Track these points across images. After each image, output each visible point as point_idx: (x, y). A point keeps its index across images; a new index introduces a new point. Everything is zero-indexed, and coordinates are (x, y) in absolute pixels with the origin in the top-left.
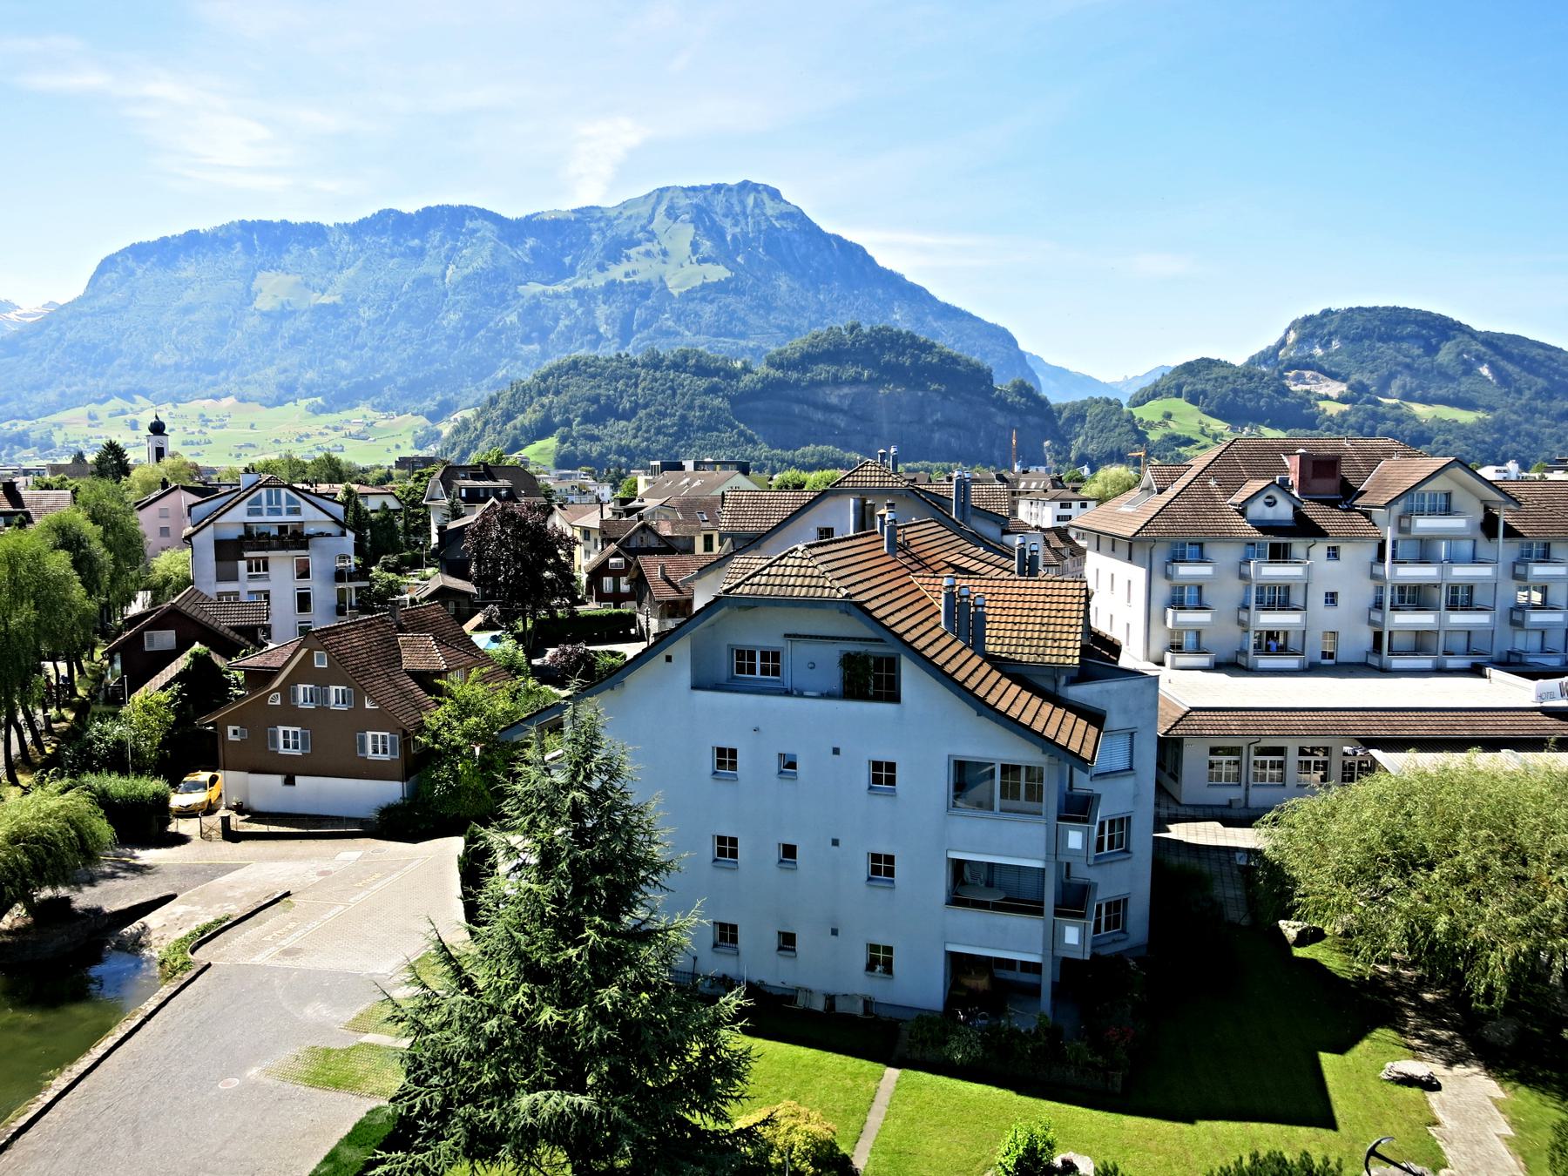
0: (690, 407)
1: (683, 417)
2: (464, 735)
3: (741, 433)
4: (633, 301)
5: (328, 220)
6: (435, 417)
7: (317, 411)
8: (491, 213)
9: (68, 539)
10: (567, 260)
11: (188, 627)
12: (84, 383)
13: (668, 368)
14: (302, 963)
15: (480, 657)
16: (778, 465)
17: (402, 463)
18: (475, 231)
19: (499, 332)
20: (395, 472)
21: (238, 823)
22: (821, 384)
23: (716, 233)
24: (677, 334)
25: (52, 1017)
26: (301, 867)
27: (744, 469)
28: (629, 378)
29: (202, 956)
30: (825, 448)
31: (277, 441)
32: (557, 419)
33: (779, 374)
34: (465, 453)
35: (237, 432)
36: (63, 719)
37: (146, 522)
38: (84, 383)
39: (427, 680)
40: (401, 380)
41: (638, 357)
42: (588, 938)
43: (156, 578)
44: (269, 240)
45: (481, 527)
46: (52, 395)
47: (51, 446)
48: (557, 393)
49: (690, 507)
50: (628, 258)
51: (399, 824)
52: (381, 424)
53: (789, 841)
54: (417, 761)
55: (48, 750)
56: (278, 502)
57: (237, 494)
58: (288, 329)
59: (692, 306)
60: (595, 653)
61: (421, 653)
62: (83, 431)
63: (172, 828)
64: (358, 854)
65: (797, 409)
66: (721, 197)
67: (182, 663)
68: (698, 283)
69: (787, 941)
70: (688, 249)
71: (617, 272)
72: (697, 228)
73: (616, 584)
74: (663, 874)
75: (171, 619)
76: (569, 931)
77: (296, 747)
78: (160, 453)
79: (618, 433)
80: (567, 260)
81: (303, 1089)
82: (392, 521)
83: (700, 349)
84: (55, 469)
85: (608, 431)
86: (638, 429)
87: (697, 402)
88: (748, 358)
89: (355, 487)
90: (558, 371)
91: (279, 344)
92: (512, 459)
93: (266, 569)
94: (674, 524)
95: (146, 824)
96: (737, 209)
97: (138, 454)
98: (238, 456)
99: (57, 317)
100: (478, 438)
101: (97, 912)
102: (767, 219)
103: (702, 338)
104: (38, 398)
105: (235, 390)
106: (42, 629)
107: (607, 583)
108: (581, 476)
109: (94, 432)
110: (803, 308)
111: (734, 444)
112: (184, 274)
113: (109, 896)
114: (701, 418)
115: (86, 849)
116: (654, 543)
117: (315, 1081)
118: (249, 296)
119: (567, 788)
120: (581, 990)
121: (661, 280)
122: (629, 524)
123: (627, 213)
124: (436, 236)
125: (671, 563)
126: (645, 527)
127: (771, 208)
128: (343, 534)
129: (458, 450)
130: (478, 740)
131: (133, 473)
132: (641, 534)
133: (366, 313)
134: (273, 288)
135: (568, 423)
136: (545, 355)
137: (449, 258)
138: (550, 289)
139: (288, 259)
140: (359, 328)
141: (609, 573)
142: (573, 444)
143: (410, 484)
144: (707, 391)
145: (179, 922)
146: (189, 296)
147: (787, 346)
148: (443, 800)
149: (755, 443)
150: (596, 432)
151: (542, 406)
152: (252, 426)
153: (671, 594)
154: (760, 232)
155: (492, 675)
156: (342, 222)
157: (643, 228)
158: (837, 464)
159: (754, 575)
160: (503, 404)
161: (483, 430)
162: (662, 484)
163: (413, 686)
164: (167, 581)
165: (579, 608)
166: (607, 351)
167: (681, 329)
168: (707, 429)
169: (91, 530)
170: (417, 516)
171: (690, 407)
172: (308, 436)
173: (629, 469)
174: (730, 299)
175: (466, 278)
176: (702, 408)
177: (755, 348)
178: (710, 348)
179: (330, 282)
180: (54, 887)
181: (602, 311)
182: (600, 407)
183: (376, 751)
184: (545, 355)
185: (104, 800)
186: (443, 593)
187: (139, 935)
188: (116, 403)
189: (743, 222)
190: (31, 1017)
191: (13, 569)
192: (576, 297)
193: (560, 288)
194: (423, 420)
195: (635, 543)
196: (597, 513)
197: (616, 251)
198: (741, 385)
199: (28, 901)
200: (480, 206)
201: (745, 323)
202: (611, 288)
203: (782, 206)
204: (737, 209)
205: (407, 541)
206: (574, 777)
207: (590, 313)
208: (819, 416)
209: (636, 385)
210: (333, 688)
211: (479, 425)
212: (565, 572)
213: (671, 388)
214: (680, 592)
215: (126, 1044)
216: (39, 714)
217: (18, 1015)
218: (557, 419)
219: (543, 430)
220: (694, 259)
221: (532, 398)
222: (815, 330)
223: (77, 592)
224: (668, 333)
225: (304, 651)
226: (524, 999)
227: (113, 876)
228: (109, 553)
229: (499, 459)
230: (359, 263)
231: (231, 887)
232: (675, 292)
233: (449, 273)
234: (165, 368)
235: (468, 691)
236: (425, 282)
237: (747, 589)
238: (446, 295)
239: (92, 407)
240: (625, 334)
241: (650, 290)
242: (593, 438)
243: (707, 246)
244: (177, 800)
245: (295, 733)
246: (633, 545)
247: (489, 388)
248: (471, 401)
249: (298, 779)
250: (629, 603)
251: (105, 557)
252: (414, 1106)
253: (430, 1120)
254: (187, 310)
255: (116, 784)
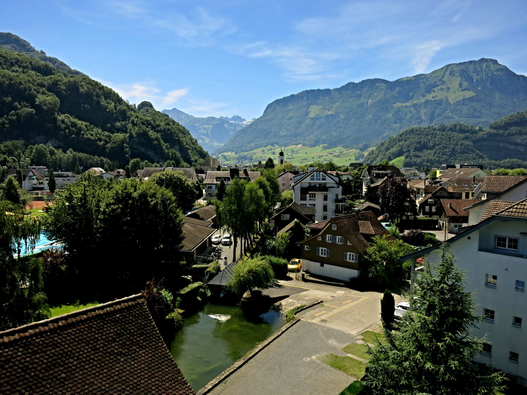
0: (457, 145)
1: (453, 149)
2: (381, 257)
3: (477, 154)
4: (435, 107)
5: (332, 88)
6: (362, 150)
7: (325, 148)
8: (384, 80)
9: (261, 185)
10: (411, 94)
11: (293, 213)
12: (261, 141)
13: (448, 130)
14: (328, 325)
15: (387, 232)
16: (493, 167)
17: (352, 165)
18: (379, 87)
19: (386, 120)
20: (349, 168)
21: (307, 276)
22: (513, 135)
23: (470, 79)
24: (452, 117)
25: (256, 326)
26: (326, 293)
27: (481, 167)
28: (433, 135)
29: (297, 316)
30: (514, 160)
31: (313, 158)
32: (405, 150)
33: (495, 131)
34: (372, 162)
35: (302, 155)
36: (257, 238)
37: (280, 181)
38: (261, 141)
39: (368, 237)
40: (352, 138)
41: (435, 127)
42: (446, 340)
43: (282, 198)
44: (312, 96)
45: (384, 186)
46: (253, 145)
47: (252, 159)
48: (405, 141)
49: (460, 181)
50: (434, 91)
51: (358, 285)
52: (345, 152)
53: (519, 316)
54: (363, 264)
55: (254, 247)
56: (319, 176)
57: (306, 174)
58: (318, 123)
59: (458, 107)
60: (424, 233)
61: (366, 228)
62: (262, 155)
63: (288, 275)
64: (343, 292)
65: (502, 145)
66: (472, 65)
67: (292, 224)
68: (462, 98)
69: (514, 356)
70: (458, 86)
71: (429, 97)
72: (462, 78)
73: (431, 209)
74: (475, 321)
75: (290, 211)
76: (438, 336)
77: (325, 254)
78: (282, 162)
79: (427, 155)
80: (411, 94)
81: (329, 367)
82: (350, 183)
83: (461, 123)
84: (255, 166)
85: (424, 154)
86: (436, 153)
87: (459, 143)
88: (481, 125)
89: (339, 172)
90: (406, 133)
91: (315, 128)
92: (391, 163)
93: (315, 197)
94: (454, 188)
95: (282, 273)
96: (479, 69)
97: (276, 162)
98: (302, 162)
99: (256, 122)
100: (377, 156)
101: (268, 297)
102: (491, 72)
103: (462, 119)
104: (250, 146)
105: (302, 142)
106: (256, 212)
107: (427, 208)
108: (414, 170)
109: (263, 155)
110: (506, 105)
111: (474, 159)
112: (289, 108)
113: (271, 292)
114: (460, 149)
115: (267, 278)
116: (446, 194)
117: (332, 365)
118: (307, 113)
119: (440, 282)
120: (441, 359)
121: (446, 98)
122: (436, 188)
123: (434, 75)
124: (365, 89)
125: (454, 202)
126: (442, 189)
127: (493, 67)
128: (338, 187)
129: (370, 161)
130: (385, 260)
131: (276, 167)
132: (440, 191)
133: (342, 116)
134: (314, 110)
135: (409, 151)
136: (401, 128)
137: (369, 97)
138: (404, 105)
139: (319, 101)
140: (339, 121)
141: (428, 205)
142: (410, 158)
143: (356, 171)
144: (463, 139)
145: (291, 304)
146: (291, 114)
147: (498, 120)
148: (372, 279)
149: (483, 158)
150: (419, 154)
151: (400, 145)
152: (306, 153)
153: (453, 214)
154: (488, 77)
155: (389, 237)
156: (336, 88)
157: (440, 80)
158: (519, 166)
159: (510, 208)
160: (386, 145)
161: (379, 154)
162: (448, 173)
163: (363, 239)
164: (285, 199)
165: (418, 217)
166: (424, 125)
167: (454, 116)
168: (463, 153)
169: (267, 183)
170: (358, 182)
171: (457, 145)
172: (322, 156)
173: (431, 167)
174: (474, 104)
175: (375, 103)
176: (461, 145)
177: (484, 121)
178: (465, 123)
179: (331, 107)
180: (258, 287)
181: (423, 111)
182: (421, 145)
183: (350, 259)
184: (401, 128)
185: (271, 263)
186: (368, 208)
187: (279, 306)
188: (270, 147)
189: (481, 74)
190: (251, 325)
191: (251, 194)
192: (413, 107)
193: (408, 104)
194: (358, 151)
195: (438, 195)
196: (423, 183)
197: (429, 90)
198: (478, 136)
199: (251, 290)
200: (381, 78)
201: (480, 112)
202: (427, 102)
203: (498, 67)
204: (479, 69)
205: (355, 190)
206: (443, 278)
207: (418, 112)
208: (512, 147)
209: (435, 137)
210: (338, 237)
211: (377, 152)
212: (413, 202)
213: (449, 138)
214: (457, 213)
215: (277, 339)
216: (252, 237)
217: (248, 323)
218: (405, 150)
219: (399, 154)
220: (460, 90)
221: (396, 143)
222: (511, 114)
223: (264, 202)
224: (448, 118)
225: (329, 224)
226: (420, 357)
227: (272, 287)
228: (272, 190)
229: (387, 163)
230: (340, 101)
231: (305, 296)
232: (452, 103)
233: (369, 101)
234: (283, 136)
235: (382, 242)
236: (362, 105)
237: (506, 213)
238: (368, 109)
239: (263, 148)
240: (432, 119)
241: (442, 102)
242: (418, 156)
243: (465, 84)
244: (290, 266)
245: (325, 250)
246: (437, 195)
247: (381, 140)
248: (375, 144)
249: (325, 265)
250: (435, 216)
251: (271, 191)
252: (373, 384)
253: (377, 390)
254: (290, 118)
255: (274, 259)
